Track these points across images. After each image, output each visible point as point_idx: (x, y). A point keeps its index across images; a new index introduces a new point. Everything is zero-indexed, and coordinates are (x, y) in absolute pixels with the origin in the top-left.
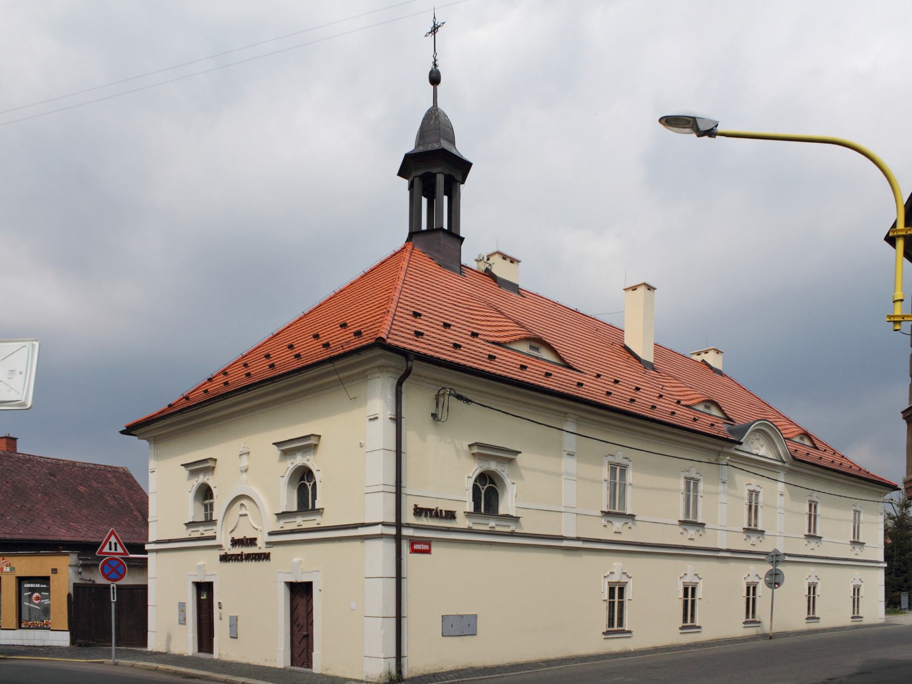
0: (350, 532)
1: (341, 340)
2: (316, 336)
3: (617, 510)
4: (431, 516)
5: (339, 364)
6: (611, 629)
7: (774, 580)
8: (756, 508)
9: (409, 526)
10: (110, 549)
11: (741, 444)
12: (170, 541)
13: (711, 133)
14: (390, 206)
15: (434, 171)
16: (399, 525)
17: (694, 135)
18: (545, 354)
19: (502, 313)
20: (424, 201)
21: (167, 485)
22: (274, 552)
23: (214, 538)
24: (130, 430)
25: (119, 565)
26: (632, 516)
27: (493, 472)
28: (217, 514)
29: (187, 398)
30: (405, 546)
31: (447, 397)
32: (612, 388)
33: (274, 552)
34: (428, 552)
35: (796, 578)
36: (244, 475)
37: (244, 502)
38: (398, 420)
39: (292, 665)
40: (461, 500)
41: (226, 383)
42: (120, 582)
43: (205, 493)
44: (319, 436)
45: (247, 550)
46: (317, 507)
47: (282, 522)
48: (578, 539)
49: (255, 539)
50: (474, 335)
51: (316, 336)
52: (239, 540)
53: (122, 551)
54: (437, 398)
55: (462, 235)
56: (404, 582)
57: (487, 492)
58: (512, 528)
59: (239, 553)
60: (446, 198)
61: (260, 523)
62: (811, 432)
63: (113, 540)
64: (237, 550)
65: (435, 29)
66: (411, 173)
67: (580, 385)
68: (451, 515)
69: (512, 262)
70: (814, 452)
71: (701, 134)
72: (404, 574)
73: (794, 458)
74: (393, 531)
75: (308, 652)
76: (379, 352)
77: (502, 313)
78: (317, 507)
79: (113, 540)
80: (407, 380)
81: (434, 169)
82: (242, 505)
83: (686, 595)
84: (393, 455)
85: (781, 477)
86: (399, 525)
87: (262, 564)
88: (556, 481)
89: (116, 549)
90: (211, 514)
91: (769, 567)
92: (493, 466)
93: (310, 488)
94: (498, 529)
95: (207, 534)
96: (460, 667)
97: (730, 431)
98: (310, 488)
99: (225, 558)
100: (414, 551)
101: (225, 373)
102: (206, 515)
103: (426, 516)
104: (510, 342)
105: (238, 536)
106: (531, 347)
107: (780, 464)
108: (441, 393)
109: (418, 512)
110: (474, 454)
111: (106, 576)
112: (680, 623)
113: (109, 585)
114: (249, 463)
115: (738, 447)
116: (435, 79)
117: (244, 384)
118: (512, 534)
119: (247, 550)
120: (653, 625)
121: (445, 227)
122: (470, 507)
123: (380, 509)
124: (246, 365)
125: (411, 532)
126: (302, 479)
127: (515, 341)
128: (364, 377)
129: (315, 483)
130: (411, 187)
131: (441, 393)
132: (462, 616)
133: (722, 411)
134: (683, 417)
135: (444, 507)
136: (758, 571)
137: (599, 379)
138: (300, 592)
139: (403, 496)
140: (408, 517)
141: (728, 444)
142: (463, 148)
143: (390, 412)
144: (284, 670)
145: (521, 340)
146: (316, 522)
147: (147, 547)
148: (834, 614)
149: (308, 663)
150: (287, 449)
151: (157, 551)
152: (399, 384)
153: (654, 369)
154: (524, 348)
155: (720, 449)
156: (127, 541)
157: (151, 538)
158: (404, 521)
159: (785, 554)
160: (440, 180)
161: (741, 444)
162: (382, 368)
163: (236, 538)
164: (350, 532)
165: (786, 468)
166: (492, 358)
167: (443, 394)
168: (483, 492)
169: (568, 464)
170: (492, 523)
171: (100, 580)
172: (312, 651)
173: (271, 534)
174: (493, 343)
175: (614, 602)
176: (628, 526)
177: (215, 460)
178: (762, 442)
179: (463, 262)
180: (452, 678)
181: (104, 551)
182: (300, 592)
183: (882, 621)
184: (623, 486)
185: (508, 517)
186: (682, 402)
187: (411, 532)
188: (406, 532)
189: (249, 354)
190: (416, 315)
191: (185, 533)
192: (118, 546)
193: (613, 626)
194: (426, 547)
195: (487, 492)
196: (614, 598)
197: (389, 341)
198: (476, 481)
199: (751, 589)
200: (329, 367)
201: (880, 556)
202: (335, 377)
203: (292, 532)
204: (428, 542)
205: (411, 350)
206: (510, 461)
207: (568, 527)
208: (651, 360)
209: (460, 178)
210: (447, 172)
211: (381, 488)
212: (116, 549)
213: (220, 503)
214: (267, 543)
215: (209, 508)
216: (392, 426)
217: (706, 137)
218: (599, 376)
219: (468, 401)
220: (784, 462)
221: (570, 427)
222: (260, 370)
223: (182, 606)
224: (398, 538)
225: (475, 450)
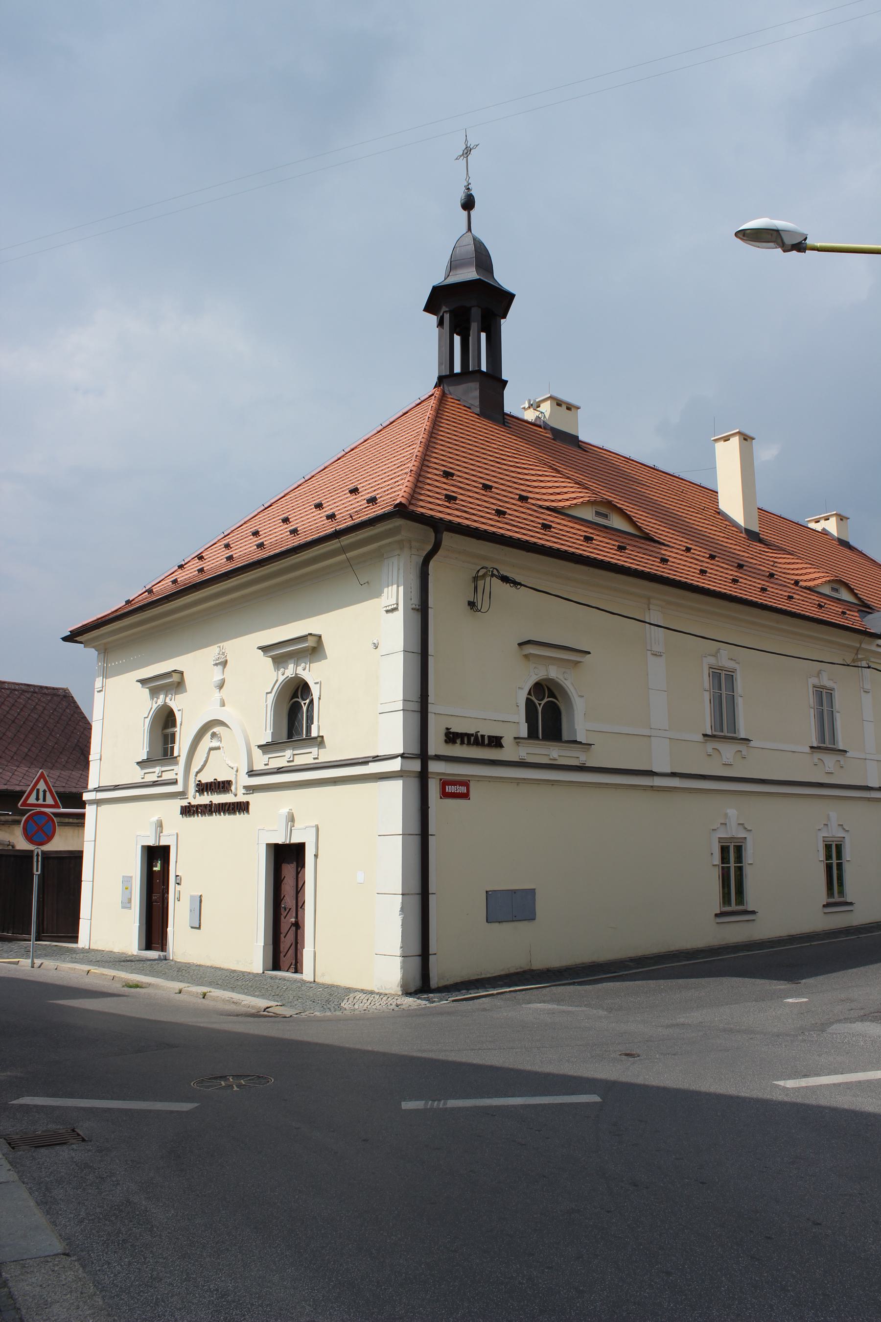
2: (319, 506)
4: (469, 743)
5: (346, 540)
9: (438, 758)
10: (37, 799)
12: (116, 788)
13: (800, 247)
14: (421, 350)
16: (424, 756)
17: (780, 250)
20: (457, 339)
21: (116, 713)
22: (254, 800)
23: (175, 782)
24: (72, 637)
25: (47, 822)
27: (552, 681)
28: (181, 747)
29: (150, 591)
31: (488, 579)
33: (254, 800)
34: (465, 796)
40: (508, 717)
41: (201, 570)
42: (47, 848)
43: (165, 722)
45: (218, 799)
48: (673, 775)
50: (523, 499)
51: (319, 506)
53: (52, 803)
54: (475, 579)
55: (504, 377)
56: (432, 899)
57: (547, 714)
60: (483, 335)
61: (228, 761)
63: (42, 786)
65: (467, 151)
66: (440, 309)
68: (496, 742)
69: (569, 409)
71: (787, 248)
72: (432, 888)
76: (398, 522)
78: (314, 734)
79: (42, 786)
81: (471, 305)
88: (640, 688)
89: (44, 800)
92: (553, 673)
93: (305, 709)
95: (166, 776)
96: (512, 970)
98: (305, 709)
99: (188, 811)
100: (445, 795)
101: (200, 557)
103: (462, 743)
105: (206, 777)
106: (598, 514)
108: (480, 574)
109: (451, 737)
111: (29, 838)
112: (823, 898)
113: (32, 851)
114: (226, 683)
116: (468, 204)
117: (224, 570)
119: (218, 799)
121: (484, 368)
124: (227, 546)
126: (295, 695)
128: (379, 556)
129: (312, 702)
130: (441, 324)
131: (480, 574)
132: (514, 892)
133: (856, 595)
135: (487, 730)
138: (287, 859)
140: (436, 745)
141: (867, 639)
142: (503, 277)
146: (312, 756)
147: (86, 797)
150: (279, 653)
151: (98, 802)
153: (761, 541)
156: (61, 790)
157: (92, 783)
158: (431, 751)
160: (476, 313)
164: (355, 772)
166: (546, 527)
167: (484, 576)
168: (540, 709)
170: (554, 753)
171: (22, 844)
179: (507, 410)
181: (29, 802)
182: (287, 859)
186: (801, 584)
188: (434, 767)
191: (137, 775)
192: (48, 794)
193: (730, 904)
194: (463, 790)
195: (547, 714)
197: (412, 508)
198: (529, 693)
200: (334, 544)
202: (343, 557)
203: (279, 771)
205: (441, 519)
208: (757, 530)
212: (44, 800)
214: (245, 787)
216: (417, 617)
217: (794, 252)
219: (516, 584)
221: (655, 616)
223: (127, 880)
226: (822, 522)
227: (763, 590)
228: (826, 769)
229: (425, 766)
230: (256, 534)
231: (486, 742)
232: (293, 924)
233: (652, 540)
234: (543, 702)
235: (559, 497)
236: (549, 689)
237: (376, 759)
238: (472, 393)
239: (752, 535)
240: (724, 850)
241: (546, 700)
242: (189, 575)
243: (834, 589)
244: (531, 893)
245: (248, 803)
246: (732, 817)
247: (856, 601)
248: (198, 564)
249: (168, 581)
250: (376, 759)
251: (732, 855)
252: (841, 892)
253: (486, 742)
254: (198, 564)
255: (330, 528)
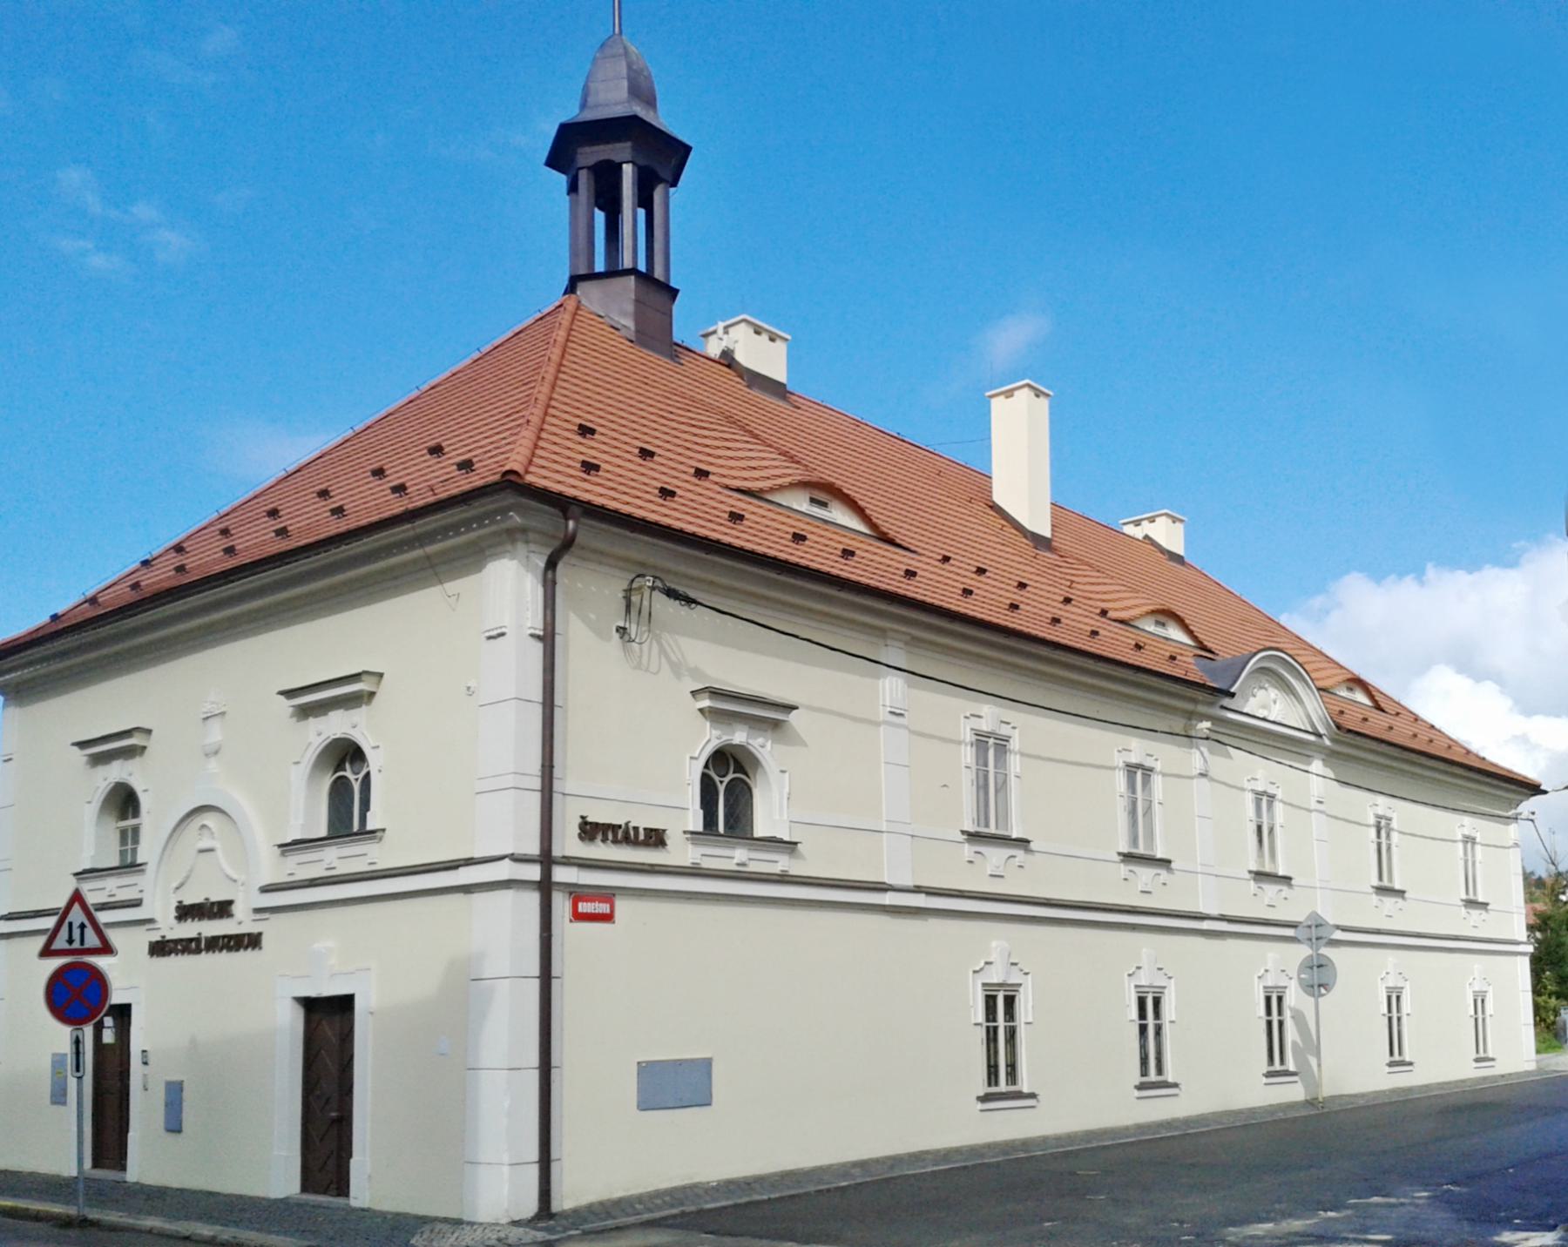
0: (445, 877)
1: (432, 480)
3: (992, 830)
4: (615, 841)
6: (993, 1089)
7: (1318, 978)
8: (1271, 830)
9: (568, 861)
11: (1233, 695)
15: (617, 159)
16: (547, 860)
18: (840, 515)
19: (756, 436)
20: (600, 217)
22: (270, 929)
23: (136, 904)
26: (1023, 843)
28: (147, 851)
29: (93, 601)
30: (561, 905)
32: (971, 581)
33: (270, 929)
34: (608, 918)
35: (1362, 976)
36: (213, 765)
37: (209, 820)
38: (548, 638)
39: (305, 1188)
41: (180, 569)
43: (124, 801)
44: (381, 675)
46: (369, 827)
47: (159, 1096)
48: (917, 890)
49: (230, 903)
50: (701, 474)
51: (379, 473)
52: (193, 906)
55: (673, 284)
57: (727, 786)
58: (780, 863)
59: (193, 935)
61: (242, 869)
62: (1365, 676)
64: (190, 929)
67: (910, 574)
68: (655, 838)
69: (772, 340)
70: (1375, 715)
73: (1339, 727)
74: (533, 873)
75: (339, 1157)
76: (509, 499)
77: (756, 436)
78: (369, 827)
80: (566, 558)
82: (204, 826)
83: (1142, 1014)
84: (536, 713)
85: (1317, 766)
86: (547, 860)
87: (245, 957)
88: (873, 753)
90: (134, 851)
91: (1303, 951)
92: (739, 736)
93: (356, 787)
94: (754, 867)
97: (1212, 673)
98: (356, 787)
99: (160, 948)
100: (578, 917)
101: (179, 548)
102: (123, 853)
103: (604, 840)
104: (771, 490)
106: (813, 500)
107: (1312, 738)
109: (590, 831)
110: (701, 710)
112: (1137, 1078)
115: (1226, 702)
117: (218, 569)
118: (783, 879)
120: (1080, 1092)
121: (642, 267)
122: (694, 819)
123: (508, 827)
124: (225, 532)
125: (574, 875)
127: (781, 488)
129: (368, 774)
130: (573, 188)
131: (635, 585)
133: (1190, 633)
134: (1114, 643)
135: (643, 821)
136: (1281, 963)
137: (946, 566)
139: (557, 798)
140: (568, 842)
143: (534, 620)
144: (285, 1202)
145: (792, 486)
148: (1442, 1061)
149: (341, 1186)
150: (310, 702)
152: (551, 564)
154: (800, 502)
155: (1189, 706)
158: (557, 852)
159: (1338, 927)
161: (1233, 695)
162: (513, 535)
163: (187, 902)
164: (445, 877)
165: (1326, 748)
166: (736, 517)
168: (721, 789)
169: (892, 688)
170: (738, 856)
172: (350, 1156)
173: (266, 890)
174: (738, 490)
175: (996, 1028)
176: (1017, 861)
177: (149, 732)
178: (1273, 693)
180: (660, 1208)
182: (328, 1019)
183: (1532, 1066)
184: (1002, 787)
185: (773, 842)
187: (574, 875)
188: (561, 874)
189: (234, 510)
190: (585, 431)
193: (997, 1084)
194: (603, 908)
195: (727, 786)
196: (995, 1020)
197: (529, 478)
198: (706, 766)
199: (1273, 1001)
201: (1521, 933)
204: (607, 895)
206: (776, 725)
207: (895, 865)
208: (1047, 533)
209: (665, 173)
210: (642, 162)
211: (510, 781)
213: (154, 821)
214: (258, 911)
215: (130, 837)
218: (946, 559)
219: (690, 601)
220: (1319, 736)
222: (256, 540)
224: (545, 887)
225: (706, 703)
226: (1145, 523)
227: (1014, 607)
228: (1138, 887)
229: (546, 874)
230: (273, 513)
231: (642, 837)
232: (334, 1121)
233: (892, 542)
234: (726, 780)
235: (756, 474)
236: (736, 761)
237: (470, 862)
238: (614, 304)
239: (1038, 541)
240: (990, 1002)
241: (731, 776)
242: (162, 576)
243: (1158, 623)
244: (704, 1067)
245: (260, 934)
246: (997, 951)
247: (1190, 642)
248: (178, 560)
249: (124, 588)
250: (470, 862)
251: (1000, 1004)
252: (1160, 1071)
253: (642, 837)
254: (178, 560)
255: (398, 506)
